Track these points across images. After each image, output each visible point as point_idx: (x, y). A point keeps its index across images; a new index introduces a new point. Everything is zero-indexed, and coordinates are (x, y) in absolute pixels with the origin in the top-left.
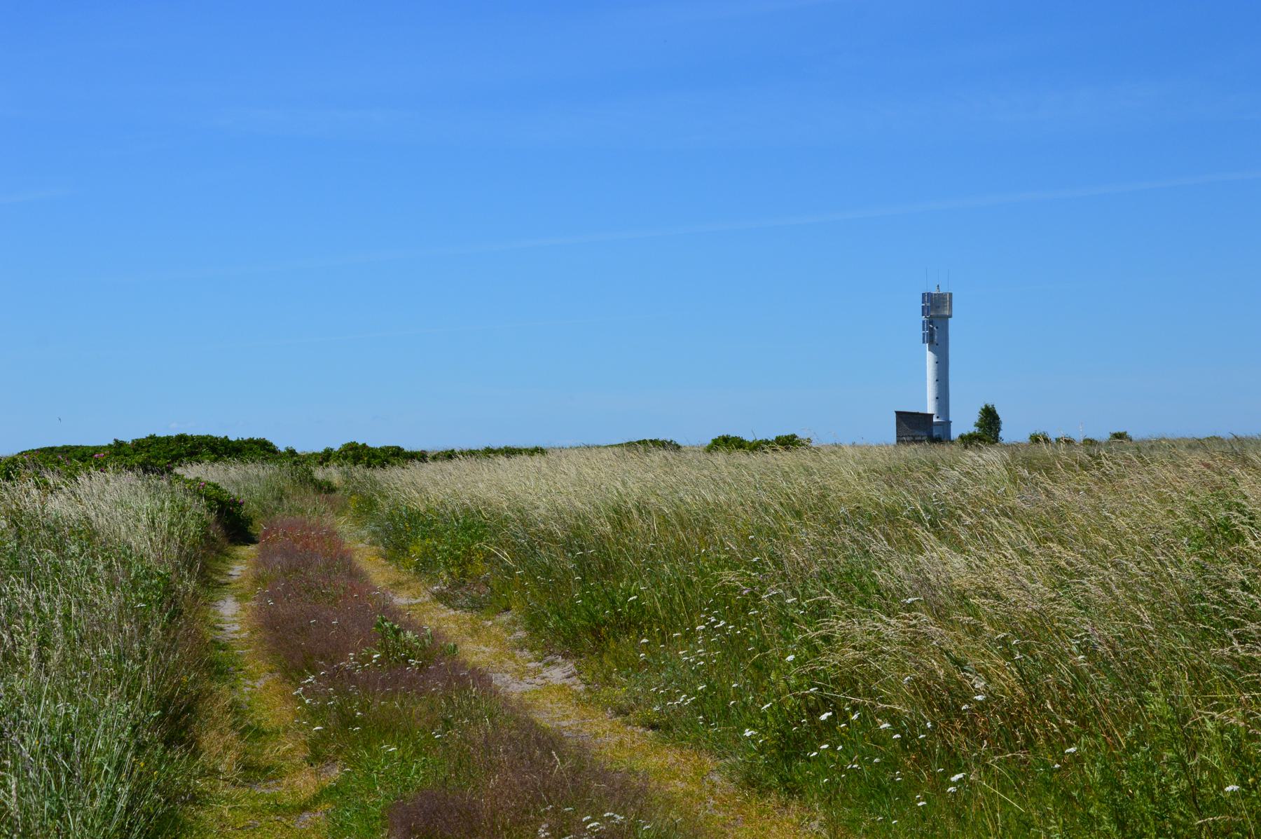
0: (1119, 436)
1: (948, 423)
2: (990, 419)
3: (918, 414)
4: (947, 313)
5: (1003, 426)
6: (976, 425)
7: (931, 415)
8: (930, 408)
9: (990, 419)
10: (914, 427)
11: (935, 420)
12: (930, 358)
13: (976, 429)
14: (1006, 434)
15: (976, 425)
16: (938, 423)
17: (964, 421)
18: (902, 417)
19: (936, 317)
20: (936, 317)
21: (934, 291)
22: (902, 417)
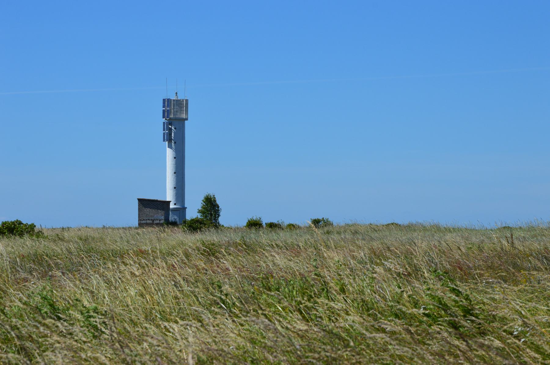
0: (316, 222)
1: (184, 209)
2: (211, 207)
3: (157, 201)
4: (184, 116)
5: (221, 213)
6: (199, 212)
7: (169, 202)
8: (169, 196)
9: (211, 207)
10: (153, 211)
11: (172, 206)
12: (170, 154)
13: (199, 216)
14: (223, 220)
15: (199, 212)
16: (174, 210)
17: (193, 212)
18: (144, 203)
19: (174, 122)
20: (174, 122)
21: (173, 98)
22: (140, 200)
